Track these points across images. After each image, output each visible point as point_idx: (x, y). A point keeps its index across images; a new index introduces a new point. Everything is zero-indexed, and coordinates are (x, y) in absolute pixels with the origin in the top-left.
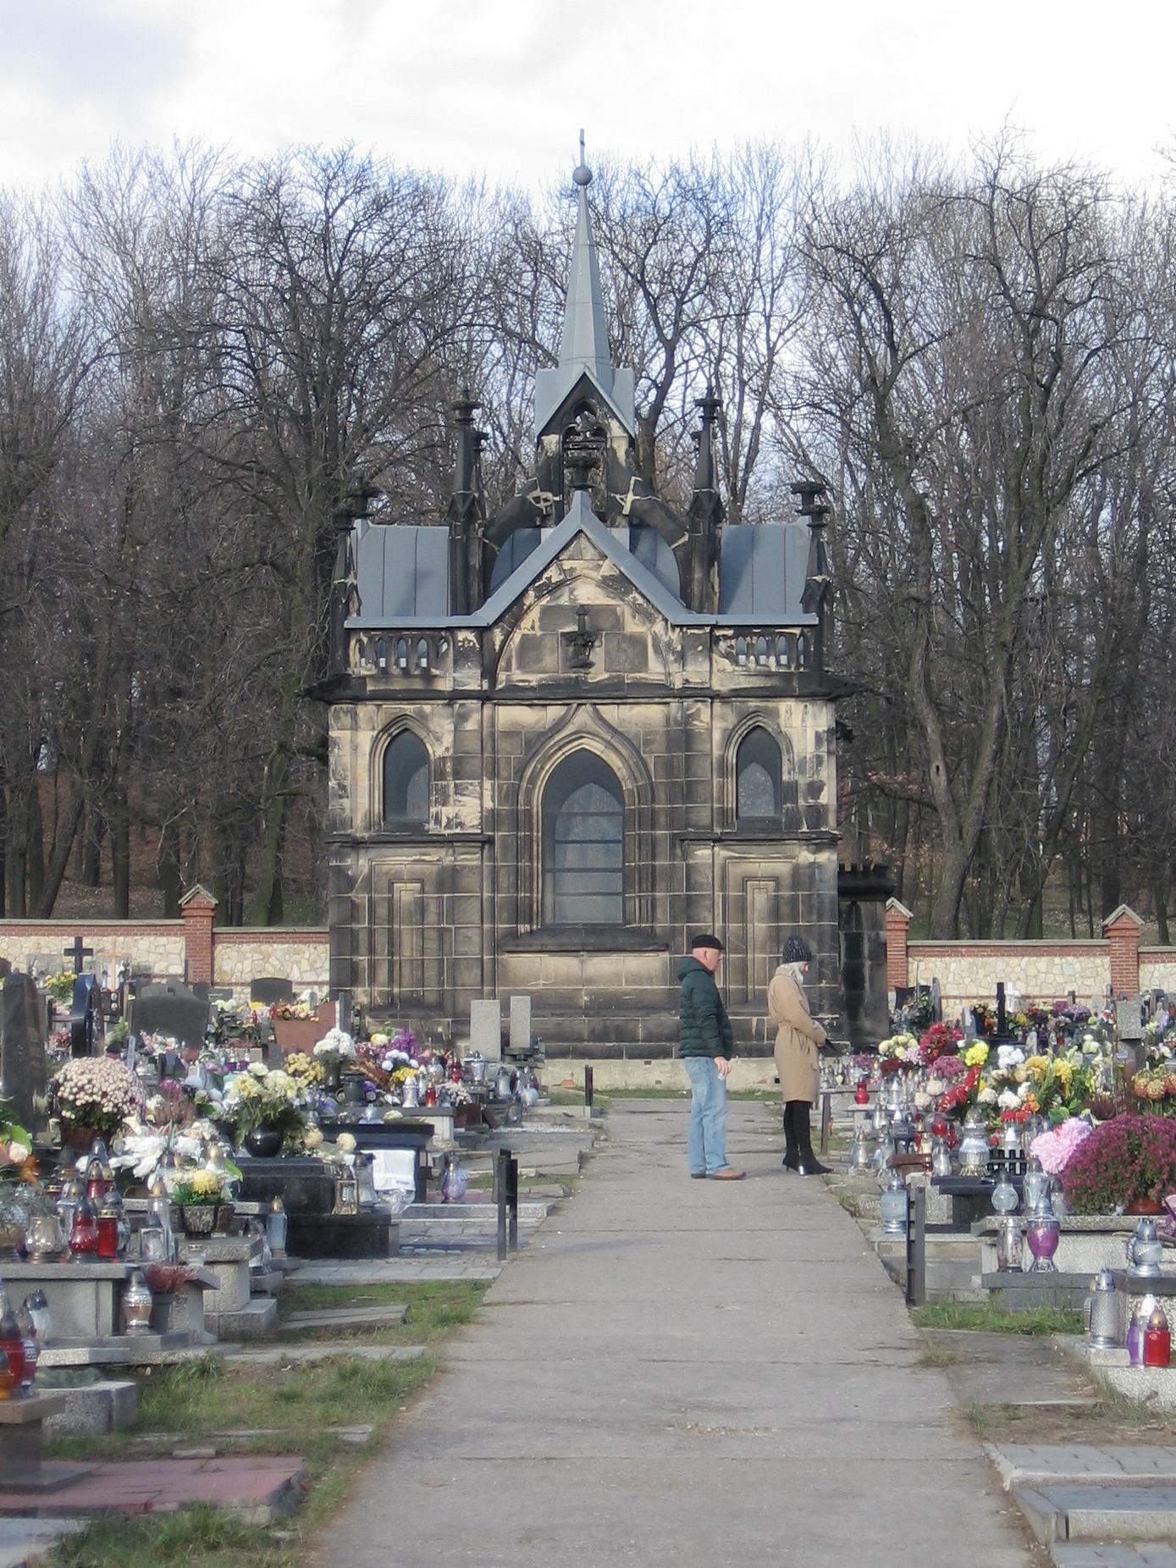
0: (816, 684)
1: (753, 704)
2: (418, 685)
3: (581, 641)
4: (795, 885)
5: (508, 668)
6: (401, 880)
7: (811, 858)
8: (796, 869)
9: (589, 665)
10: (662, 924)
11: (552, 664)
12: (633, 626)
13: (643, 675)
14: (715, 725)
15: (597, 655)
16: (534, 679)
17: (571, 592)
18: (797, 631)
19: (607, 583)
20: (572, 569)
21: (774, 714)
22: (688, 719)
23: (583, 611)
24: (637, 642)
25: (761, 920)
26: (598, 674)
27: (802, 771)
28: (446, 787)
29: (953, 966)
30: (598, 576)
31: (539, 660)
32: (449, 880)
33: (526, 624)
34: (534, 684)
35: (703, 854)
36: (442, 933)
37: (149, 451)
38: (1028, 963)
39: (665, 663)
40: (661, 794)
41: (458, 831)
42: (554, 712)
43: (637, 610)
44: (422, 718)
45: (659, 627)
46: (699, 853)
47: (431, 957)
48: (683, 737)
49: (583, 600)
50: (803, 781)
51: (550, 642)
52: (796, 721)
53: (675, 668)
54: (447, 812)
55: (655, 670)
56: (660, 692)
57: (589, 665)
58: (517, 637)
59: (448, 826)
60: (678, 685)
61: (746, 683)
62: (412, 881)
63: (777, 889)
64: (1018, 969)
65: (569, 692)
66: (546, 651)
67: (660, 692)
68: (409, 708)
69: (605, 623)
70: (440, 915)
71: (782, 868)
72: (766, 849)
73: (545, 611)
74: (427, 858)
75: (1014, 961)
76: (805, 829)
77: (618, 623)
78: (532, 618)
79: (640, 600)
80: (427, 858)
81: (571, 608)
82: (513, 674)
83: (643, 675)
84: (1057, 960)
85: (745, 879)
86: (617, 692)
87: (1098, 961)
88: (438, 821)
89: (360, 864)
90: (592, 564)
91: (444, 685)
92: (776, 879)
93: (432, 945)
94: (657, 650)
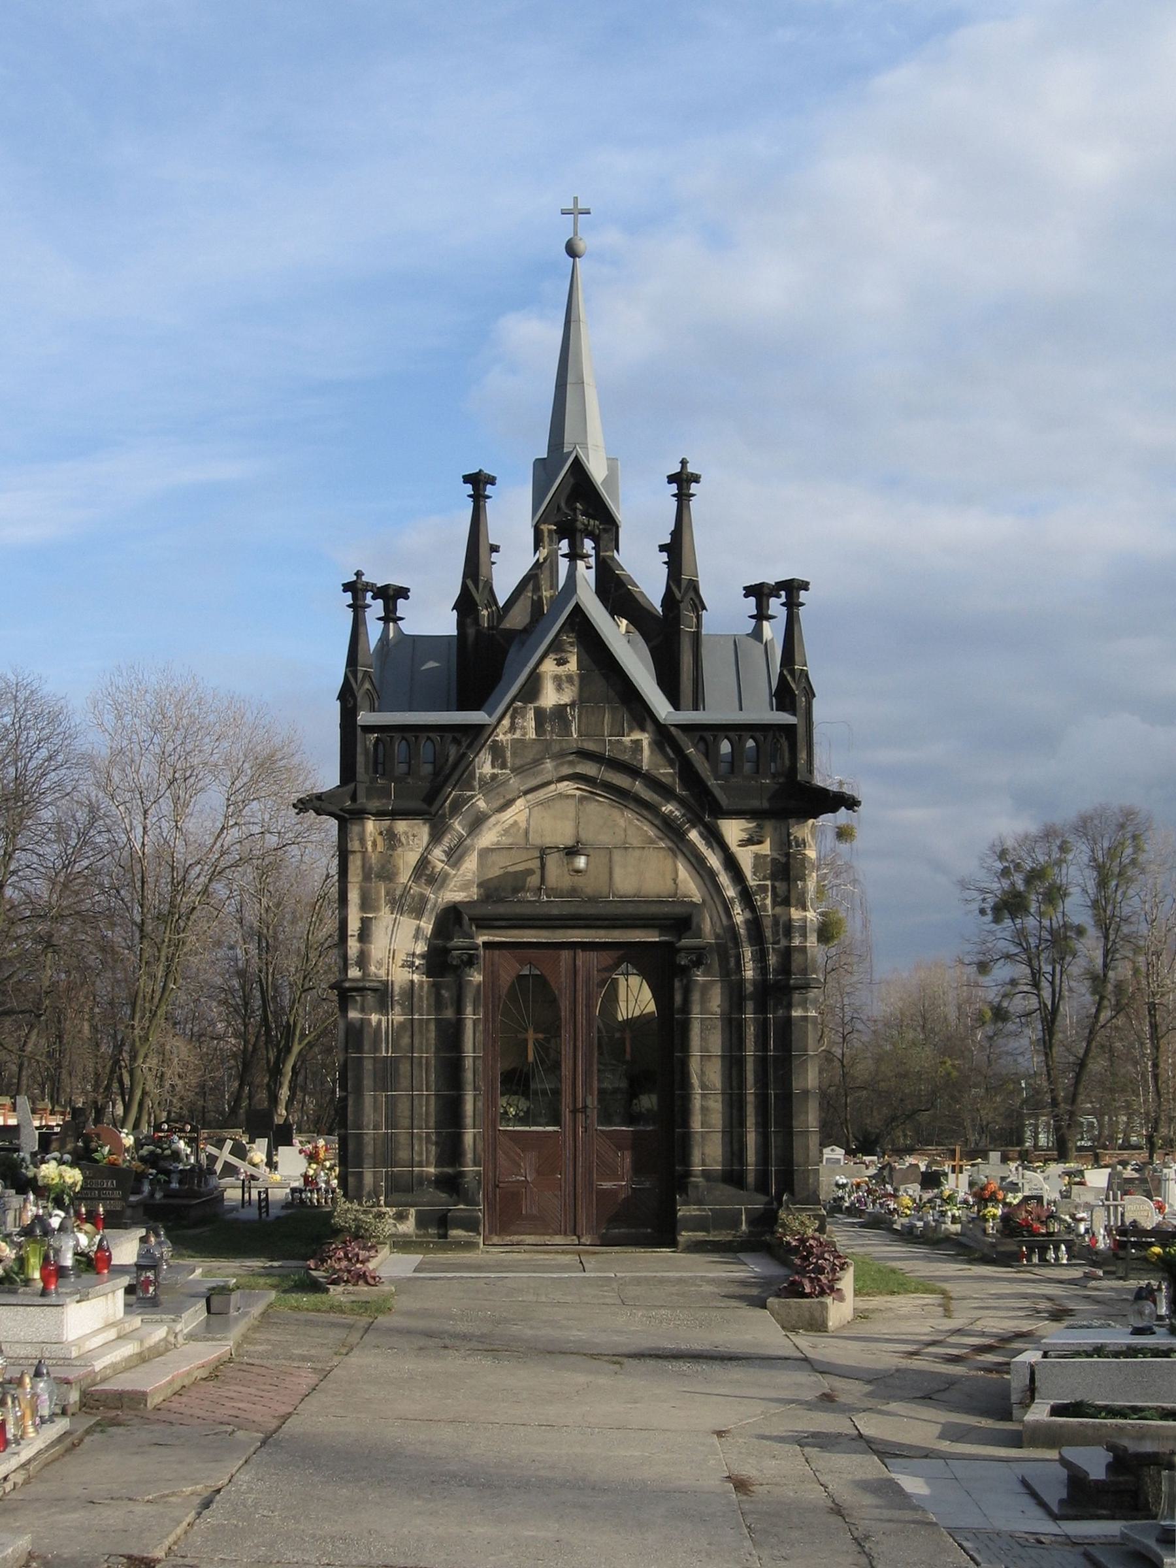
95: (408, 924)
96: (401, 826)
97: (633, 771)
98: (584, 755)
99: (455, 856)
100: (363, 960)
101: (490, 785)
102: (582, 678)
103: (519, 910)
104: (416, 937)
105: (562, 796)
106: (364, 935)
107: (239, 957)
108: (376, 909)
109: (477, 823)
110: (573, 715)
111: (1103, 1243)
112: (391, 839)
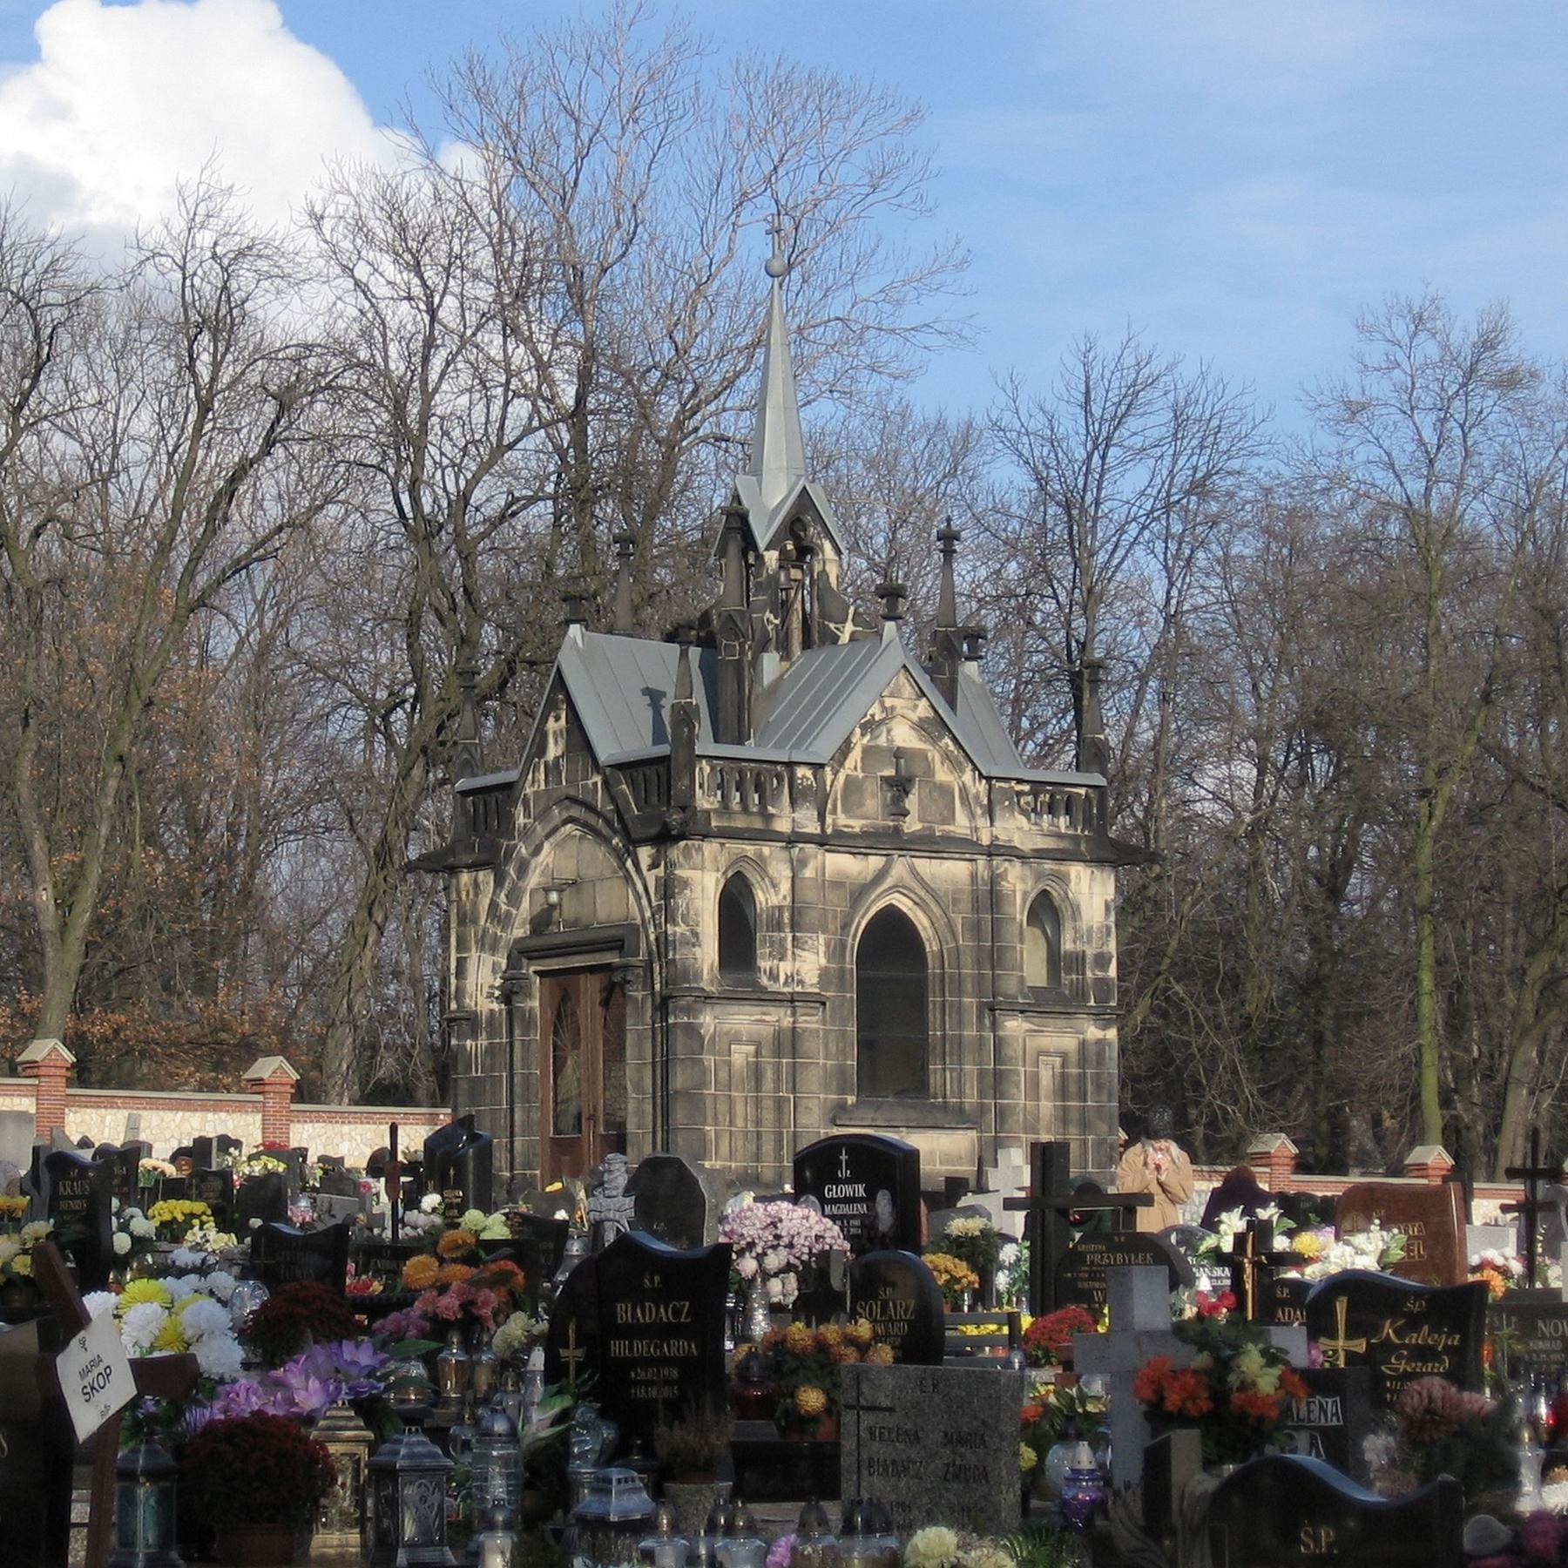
0: (1111, 854)
1: (1049, 866)
2: (758, 824)
3: (899, 786)
4: (1083, 1060)
5: (834, 811)
6: (739, 1042)
7: (1099, 1034)
8: (1083, 1045)
9: (905, 814)
10: (971, 1099)
11: (869, 814)
12: (943, 774)
13: (951, 828)
14: (1018, 883)
15: (911, 803)
16: (857, 825)
17: (889, 731)
18: (1082, 791)
19: (921, 726)
20: (893, 708)
21: (1063, 879)
22: (994, 880)
23: (898, 754)
24: (945, 791)
25: (1047, 1099)
26: (912, 825)
27: (1089, 941)
28: (782, 941)
29: (108, 1118)
30: (915, 717)
31: (861, 805)
32: (788, 1043)
33: (849, 763)
34: (857, 830)
35: (1014, 1026)
36: (779, 1103)
37: (1226, 636)
38: (182, 1119)
39: (972, 816)
40: (968, 959)
41: (799, 989)
42: (875, 862)
43: (947, 756)
44: (760, 863)
45: (968, 776)
46: (1008, 1024)
47: (768, 1128)
48: (990, 897)
49: (899, 743)
50: (1090, 952)
51: (872, 787)
52: (1084, 887)
53: (983, 822)
54: (785, 968)
55: (961, 824)
56: (964, 847)
57: (905, 814)
58: (841, 777)
59: (786, 983)
60: (986, 840)
61: (1050, 844)
62: (749, 1042)
63: (1063, 1066)
64: (172, 1126)
65: (887, 840)
66: (867, 794)
67: (964, 847)
68: (749, 849)
69: (918, 769)
70: (778, 1081)
71: (1069, 1043)
72: (1060, 1022)
73: (867, 751)
74: (767, 1018)
75: (168, 1115)
76: (1092, 1003)
77: (929, 771)
78: (855, 755)
79: (952, 747)
80: (767, 1018)
81: (889, 749)
82: (840, 820)
83: (951, 828)
84: (210, 1116)
85: (1041, 1053)
86: (933, 845)
87: (250, 1118)
88: (774, 977)
89: (708, 1020)
90: (910, 704)
91: (783, 826)
92: (1064, 1056)
93: (769, 1116)
94: (965, 800)
95: (488, 959)
96: (481, 875)
97: (591, 808)
98: (573, 800)
99: (514, 898)
100: (460, 993)
101: (526, 833)
102: (568, 730)
103: (557, 941)
104: (494, 972)
105: (569, 836)
106: (461, 972)
107: (1170, 951)
108: (468, 950)
109: (523, 869)
110: (563, 762)
111: (1113, 833)
112: (476, 885)
